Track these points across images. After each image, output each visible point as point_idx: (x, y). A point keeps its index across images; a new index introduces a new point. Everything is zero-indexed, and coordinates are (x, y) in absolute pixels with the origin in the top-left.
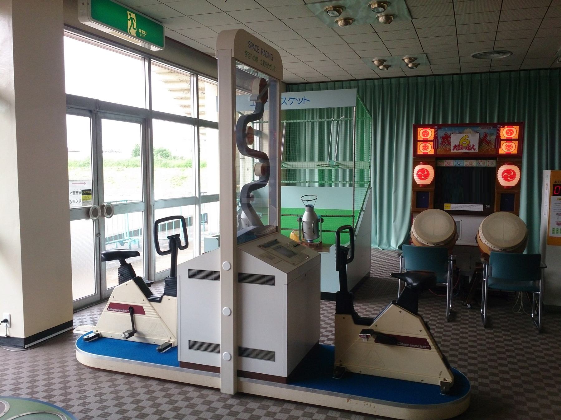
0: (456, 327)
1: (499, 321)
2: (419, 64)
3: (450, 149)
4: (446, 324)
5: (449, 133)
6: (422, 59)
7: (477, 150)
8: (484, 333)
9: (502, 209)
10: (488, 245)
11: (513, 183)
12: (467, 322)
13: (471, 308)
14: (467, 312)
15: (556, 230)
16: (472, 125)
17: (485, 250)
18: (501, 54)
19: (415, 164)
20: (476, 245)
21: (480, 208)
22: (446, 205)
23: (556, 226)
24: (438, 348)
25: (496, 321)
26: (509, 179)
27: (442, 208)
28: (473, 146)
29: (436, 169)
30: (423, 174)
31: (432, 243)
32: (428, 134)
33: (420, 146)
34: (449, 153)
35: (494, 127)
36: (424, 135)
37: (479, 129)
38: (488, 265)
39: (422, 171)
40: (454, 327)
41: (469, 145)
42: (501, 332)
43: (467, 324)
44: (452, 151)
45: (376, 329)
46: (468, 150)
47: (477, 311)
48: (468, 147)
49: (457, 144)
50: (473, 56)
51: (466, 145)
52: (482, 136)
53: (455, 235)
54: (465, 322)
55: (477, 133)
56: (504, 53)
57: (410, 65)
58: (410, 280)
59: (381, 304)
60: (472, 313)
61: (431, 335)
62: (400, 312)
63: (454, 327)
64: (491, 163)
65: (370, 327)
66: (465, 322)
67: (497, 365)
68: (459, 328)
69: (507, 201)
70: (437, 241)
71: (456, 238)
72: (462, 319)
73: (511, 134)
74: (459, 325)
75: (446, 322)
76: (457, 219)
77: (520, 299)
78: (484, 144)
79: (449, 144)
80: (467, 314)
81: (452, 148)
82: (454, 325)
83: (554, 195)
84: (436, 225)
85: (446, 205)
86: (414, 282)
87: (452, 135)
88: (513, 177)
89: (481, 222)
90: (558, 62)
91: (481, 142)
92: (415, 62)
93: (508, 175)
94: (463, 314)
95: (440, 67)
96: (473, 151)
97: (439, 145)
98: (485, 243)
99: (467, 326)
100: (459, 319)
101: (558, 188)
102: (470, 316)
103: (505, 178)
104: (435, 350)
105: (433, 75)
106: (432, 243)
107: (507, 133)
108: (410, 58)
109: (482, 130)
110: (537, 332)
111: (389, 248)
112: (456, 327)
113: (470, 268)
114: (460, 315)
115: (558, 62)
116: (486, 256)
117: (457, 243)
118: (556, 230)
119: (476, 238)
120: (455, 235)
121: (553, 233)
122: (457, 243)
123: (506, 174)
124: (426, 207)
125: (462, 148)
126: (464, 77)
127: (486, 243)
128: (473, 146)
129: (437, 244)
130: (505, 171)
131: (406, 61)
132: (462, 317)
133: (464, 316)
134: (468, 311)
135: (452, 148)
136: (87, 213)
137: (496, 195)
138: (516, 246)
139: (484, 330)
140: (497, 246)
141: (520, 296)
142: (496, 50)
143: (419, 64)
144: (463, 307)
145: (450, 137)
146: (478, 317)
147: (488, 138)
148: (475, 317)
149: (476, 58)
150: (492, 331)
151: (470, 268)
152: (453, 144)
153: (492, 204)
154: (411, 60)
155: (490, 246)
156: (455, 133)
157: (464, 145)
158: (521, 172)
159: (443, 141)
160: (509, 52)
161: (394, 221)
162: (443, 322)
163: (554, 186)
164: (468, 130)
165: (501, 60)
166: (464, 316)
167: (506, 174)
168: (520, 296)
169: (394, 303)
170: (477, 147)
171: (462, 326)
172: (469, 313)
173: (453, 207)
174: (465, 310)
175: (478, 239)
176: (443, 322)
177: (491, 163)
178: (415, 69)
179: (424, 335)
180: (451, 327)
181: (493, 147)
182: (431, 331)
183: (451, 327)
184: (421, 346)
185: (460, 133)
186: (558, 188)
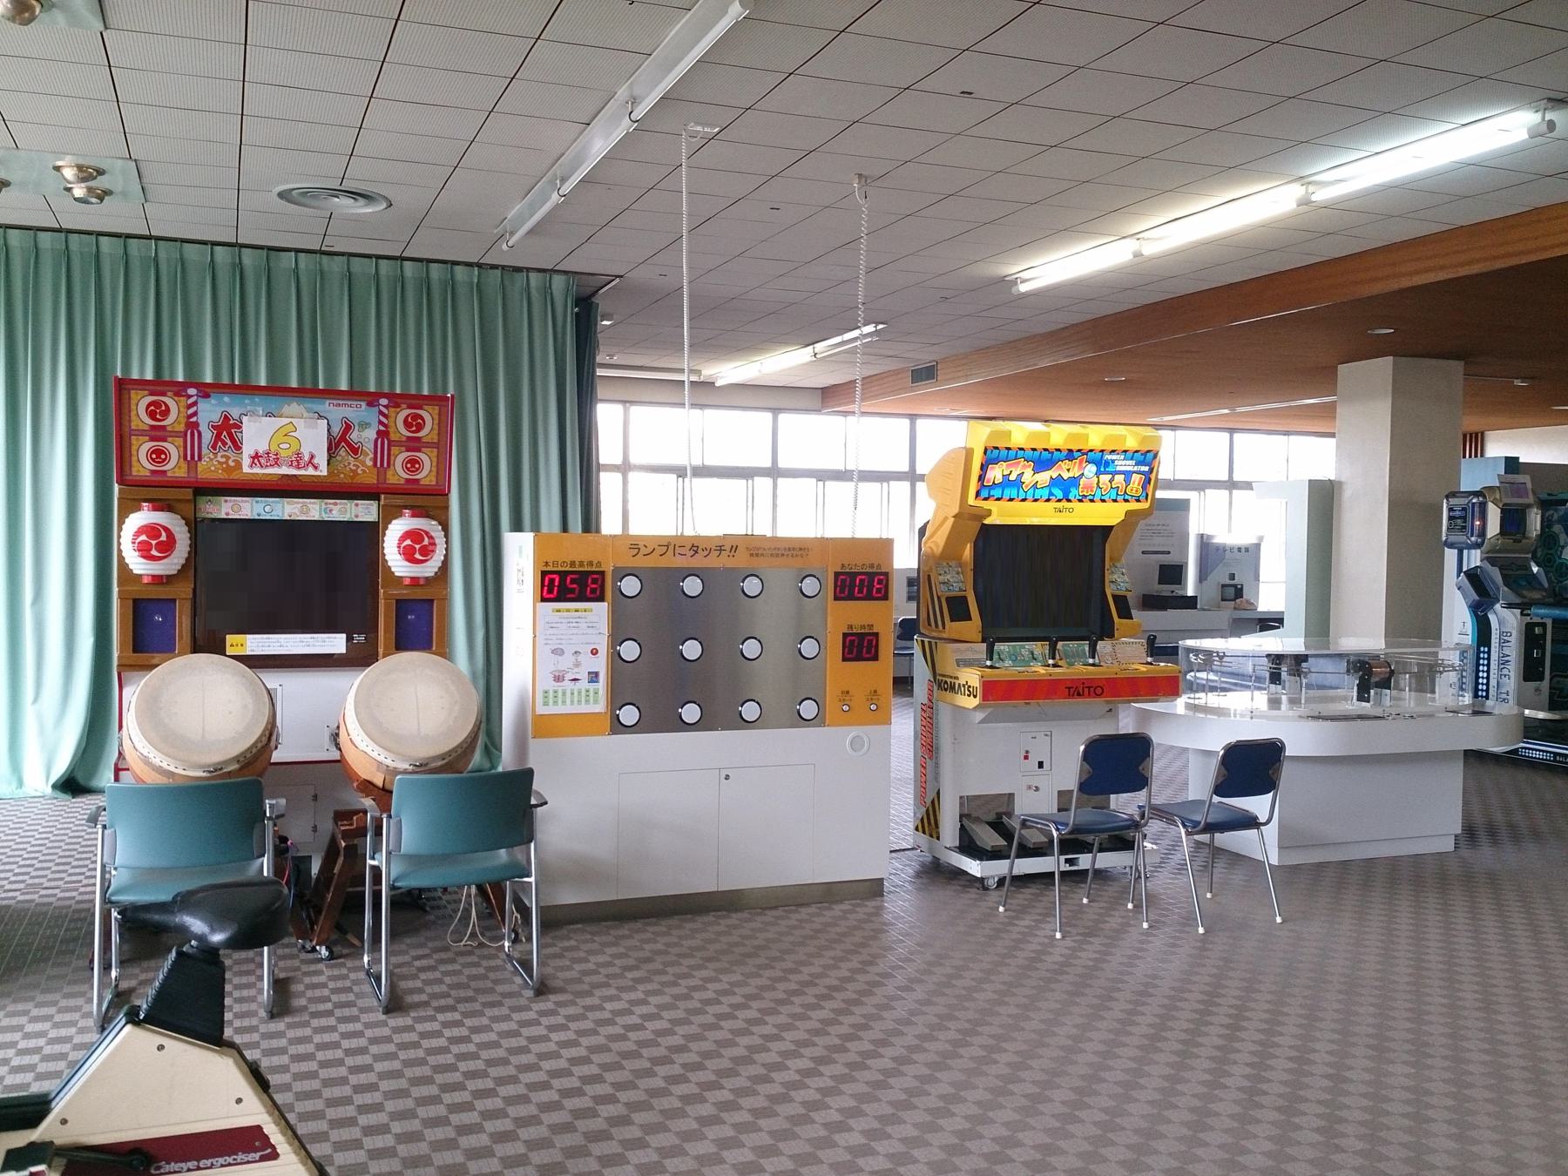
0: (300, 1032)
1: (418, 984)
2: (107, 193)
3: (239, 465)
4: (263, 1028)
5: (235, 413)
6: (118, 177)
7: (323, 471)
8: (386, 1031)
9: (402, 644)
10: (374, 755)
11: (430, 569)
12: (329, 1006)
13: (332, 957)
14: (320, 973)
15: (551, 694)
16: (307, 392)
17: (365, 771)
18: (362, 201)
19: (128, 507)
20: (335, 755)
21: (335, 643)
22: (230, 639)
23: (551, 685)
24: (300, 1143)
25: (411, 984)
26: (418, 556)
27: (219, 649)
28: (312, 457)
29: (196, 526)
30: (155, 543)
31: (200, 767)
32: (167, 412)
33: (142, 450)
34: (235, 476)
35: (370, 404)
36: (152, 415)
37: (326, 406)
38: (390, 817)
39: (151, 530)
40: (291, 1034)
41: (299, 454)
42: (433, 1019)
43: (329, 1013)
44: (246, 469)
45: (62, 1137)
46: (298, 467)
47: (349, 963)
48: (297, 460)
49: (262, 449)
50: (281, 195)
51: (289, 453)
52: (336, 430)
53: (270, 736)
54: (322, 1007)
55: (320, 417)
56: (367, 197)
57: (79, 192)
58: (197, 925)
59: (25, 1000)
60: (336, 972)
61: (279, 1112)
62: (161, 1048)
63: (291, 1034)
64: (365, 511)
65: (35, 1135)
66: (322, 1007)
67: (452, 1135)
68: (308, 1032)
69: (417, 624)
70: (216, 758)
71: (273, 744)
72: (310, 1000)
73: (420, 428)
74: (306, 1024)
75: (262, 1021)
76: (273, 679)
77: (467, 911)
78: (343, 452)
79: (237, 446)
80: (322, 979)
81: (246, 461)
82: (289, 1026)
83: (543, 600)
84: (200, 708)
85: (230, 639)
86: (213, 930)
87: (245, 419)
88: (427, 552)
89: (352, 683)
90: (504, 247)
91: (333, 447)
92: (101, 183)
93: (416, 547)
94: (307, 980)
95: (187, 208)
96: (311, 471)
97: (205, 451)
98: (367, 753)
99: (332, 1021)
100: (303, 1002)
101: (552, 581)
102: (331, 985)
103: (409, 555)
104: (293, 1158)
105: (149, 237)
106: (200, 767)
107: (407, 424)
108: (80, 168)
109: (339, 412)
110: (529, 993)
111: (20, 793)
112: (300, 1032)
113: (315, 829)
114: (300, 987)
115: (504, 247)
116: (383, 795)
117: (276, 757)
118: (551, 694)
119: (335, 737)
120: (270, 736)
121: (546, 704)
122: (276, 757)
123: (408, 542)
124: (167, 648)
125: (277, 463)
126: (248, 257)
127: (368, 750)
128: (312, 457)
129: (217, 769)
130: (408, 535)
131: (69, 173)
132: (309, 993)
133: (314, 986)
134: (321, 966)
135: (246, 461)
136: (922, 478)
137: (382, 603)
138: (454, 750)
139: (385, 1024)
140: (404, 758)
141: (469, 895)
142: (347, 185)
143: (107, 193)
144: (304, 956)
145: (238, 426)
146: (356, 982)
147: (354, 436)
148: (348, 983)
149: (289, 201)
150: (409, 1021)
151: (315, 829)
152: (248, 450)
153: (371, 628)
154: (87, 174)
155: (381, 759)
156: (254, 413)
157: (283, 454)
158: (446, 536)
159: (218, 437)
160: (386, 198)
161: (35, 700)
162: (254, 1022)
163: (544, 574)
164: (294, 407)
165: (358, 219)
166: (314, 986)
167: (408, 542)
168: (469, 895)
169: (133, 1018)
170: (322, 460)
171: (315, 1023)
172: (328, 972)
173: (257, 644)
174: (313, 968)
175: (343, 738)
176: (254, 1022)
177: (365, 511)
178: (95, 207)
179: (252, 1112)
180: (280, 1035)
181: (369, 463)
182: (275, 1097)
183: (280, 1035)
184: (241, 1157)
185: (270, 414)
186: (552, 581)
